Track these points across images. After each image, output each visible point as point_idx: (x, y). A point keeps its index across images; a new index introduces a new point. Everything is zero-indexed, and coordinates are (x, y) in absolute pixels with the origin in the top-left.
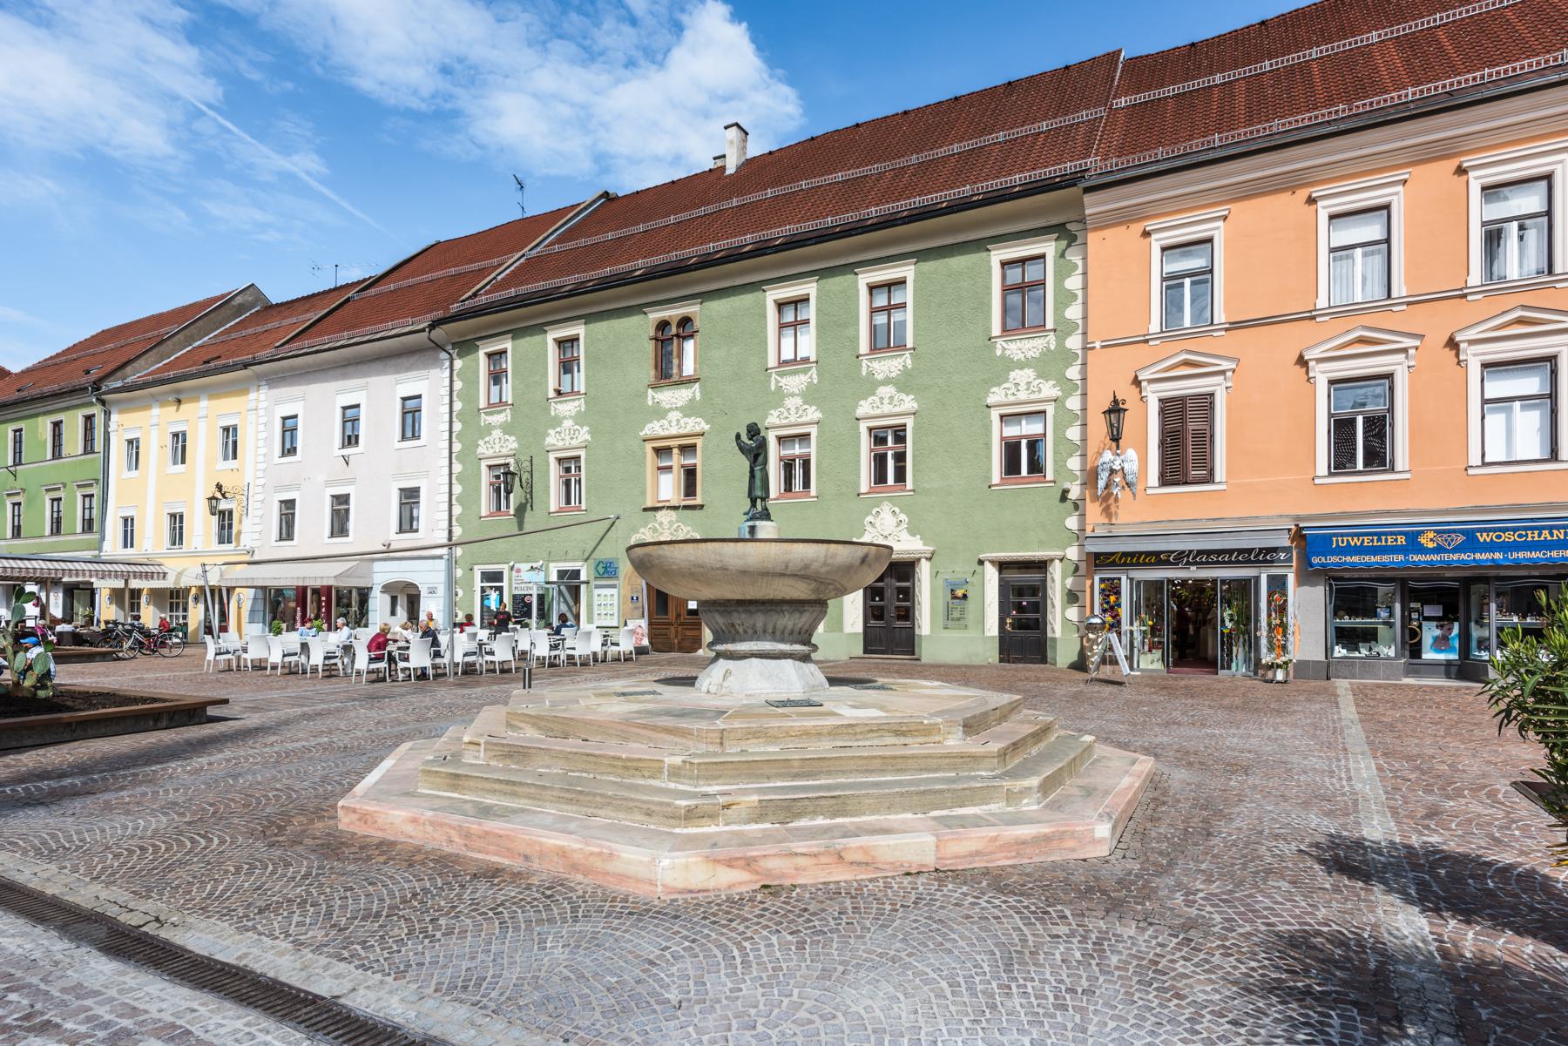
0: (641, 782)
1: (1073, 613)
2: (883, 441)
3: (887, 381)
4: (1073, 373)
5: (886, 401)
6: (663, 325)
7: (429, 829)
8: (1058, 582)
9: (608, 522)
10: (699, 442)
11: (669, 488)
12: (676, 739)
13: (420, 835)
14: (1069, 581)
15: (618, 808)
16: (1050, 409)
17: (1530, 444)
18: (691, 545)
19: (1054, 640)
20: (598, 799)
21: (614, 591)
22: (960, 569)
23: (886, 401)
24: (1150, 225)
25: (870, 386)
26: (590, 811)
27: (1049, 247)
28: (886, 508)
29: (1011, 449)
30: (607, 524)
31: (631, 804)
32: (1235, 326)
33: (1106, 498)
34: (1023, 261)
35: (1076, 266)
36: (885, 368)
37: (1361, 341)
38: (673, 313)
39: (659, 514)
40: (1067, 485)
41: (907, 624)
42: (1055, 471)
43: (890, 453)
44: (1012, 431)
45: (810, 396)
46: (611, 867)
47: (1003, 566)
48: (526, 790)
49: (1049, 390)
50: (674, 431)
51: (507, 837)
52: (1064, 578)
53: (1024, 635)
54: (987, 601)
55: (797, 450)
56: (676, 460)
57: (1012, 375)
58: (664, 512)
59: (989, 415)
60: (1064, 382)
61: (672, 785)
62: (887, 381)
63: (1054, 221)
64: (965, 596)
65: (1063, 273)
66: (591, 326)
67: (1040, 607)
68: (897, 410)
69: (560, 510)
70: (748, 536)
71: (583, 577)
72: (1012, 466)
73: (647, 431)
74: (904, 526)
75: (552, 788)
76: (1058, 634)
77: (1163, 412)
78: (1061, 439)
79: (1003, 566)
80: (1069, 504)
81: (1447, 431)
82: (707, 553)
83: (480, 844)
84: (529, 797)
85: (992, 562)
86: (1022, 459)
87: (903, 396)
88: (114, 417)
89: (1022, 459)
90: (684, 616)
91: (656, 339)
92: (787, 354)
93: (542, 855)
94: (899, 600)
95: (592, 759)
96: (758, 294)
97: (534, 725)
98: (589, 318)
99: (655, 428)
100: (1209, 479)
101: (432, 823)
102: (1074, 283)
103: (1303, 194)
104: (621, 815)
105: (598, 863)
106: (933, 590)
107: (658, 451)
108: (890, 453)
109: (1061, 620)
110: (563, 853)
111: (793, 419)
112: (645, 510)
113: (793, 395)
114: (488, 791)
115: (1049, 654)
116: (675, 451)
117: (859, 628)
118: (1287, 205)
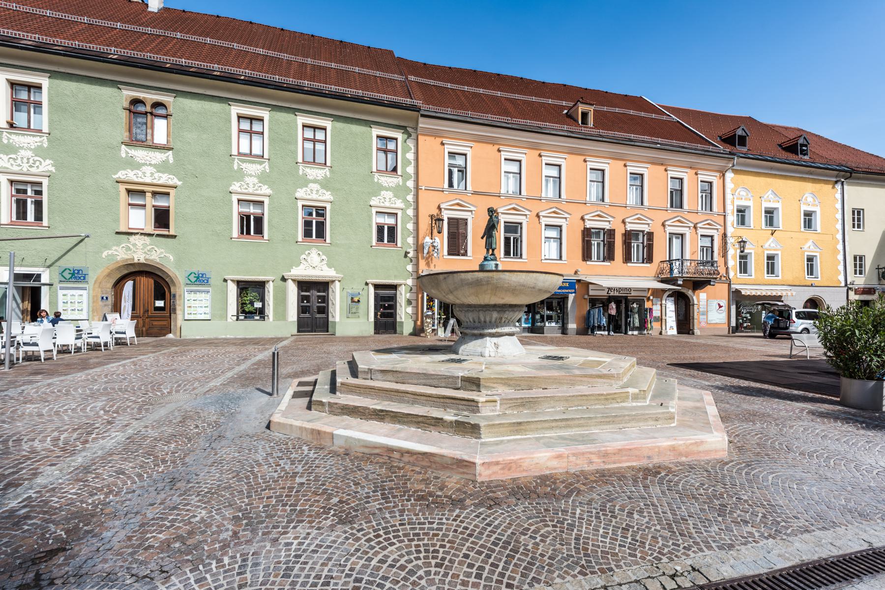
0: (617, 405)
1: (410, 310)
2: (311, 214)
3: (315, 181)
4: (410, 198)
5: (314, 192)
6: (136, 102)
7: (572, 459)
8: (403, 296)
9: (80, 239)
10: (172, 192)
12: (604, 381)
13: (565, 465)
14: (408, 295)
16: (400, 213)
19: (402, 323)
20: (627, 418)
21: (84, 293)
22: (357, 287)
23: (314, 192)
25: (305, 182)
26: (621, 426)
27: (399, 135)
28: (314, 253)
29: (380, 229)
30: (75, 240)
32: (475, 193)
33: (427, 259)
37: (458, 204)
38: (151, 97)
40: (408, 250)
42: (402, 243)
43: (29, 201)
45: (263, 178)
47: (377, 287)
48: (577, 422)
49: (399, 204)
50: (148, 180)
51: (635, 449)
53: (386, 320)
56: (150, 201)
57: (382, 193)
58: (138, 236)
59: (231, 197)
60: (406, 201)
61: (634, 404)
62: (315, 181)
66: (273, 113)
67: (393, 307)
68: (321, 198)
69: (12, 223)
71: (45, 279)
72: (380, 239)
73: (121, 175)
74: (325, 262)
75: (596, 418)
76: (337, 319)
77: (449, 224)
78: (404, 228)
79: (377, 287)
80: (408, 259)
81: (536, 248)
83: (616, 458)
84: (579, 426)
85: (233, 281)
87: (325, 191)
88: (845, 187)
89: (252, 225)
90: (152, 312)
91: (130, 111)
92: (245, 149)
94: (319, 302)
95: (584, 398)
96: (225, 106)
97: (505, 384)
98: (53, 75)
99: (130, 175)
100: (465, 254)
101: (574, 455)
102: (410, 156)
103: (496, 147)
104: (641, 424)
105: (695, 449)
106: (341, 297)
109: (405, 314)
110: (673, 449)
112: (117, 233)
113: (251, 176)
114: (547, 428)
115: (398, 329)
116: (149, 195)
117: (295, 318)
118: (491, 149)
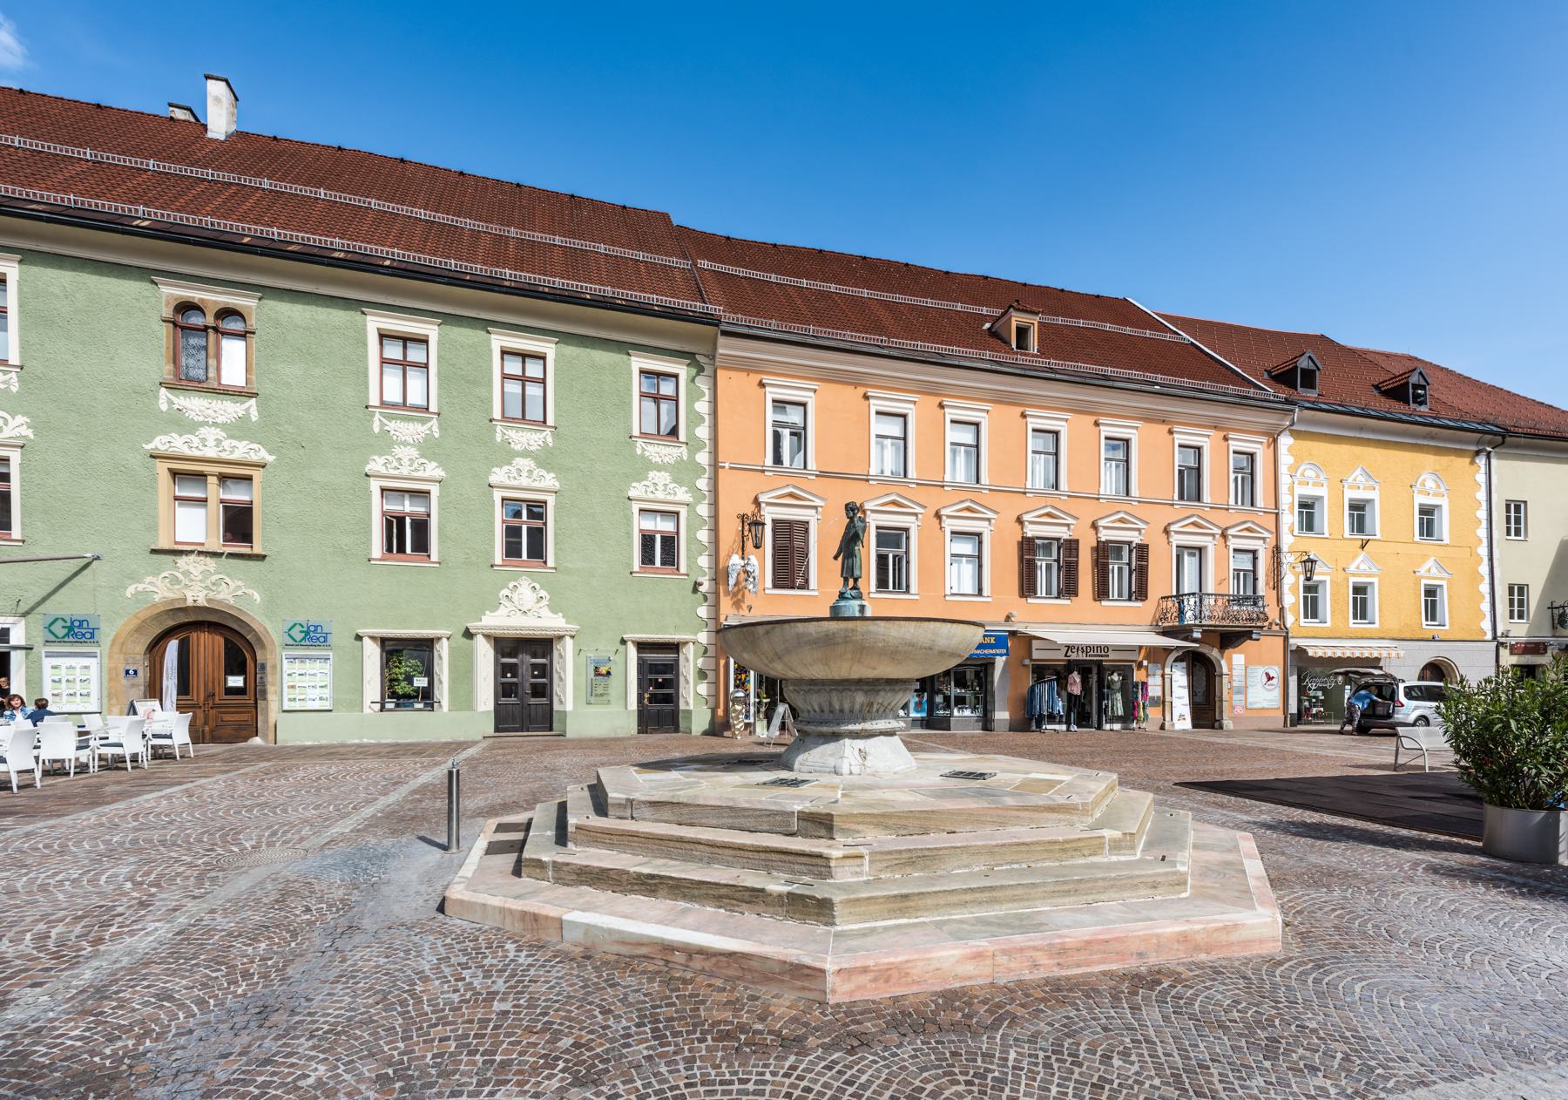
0: (1082, 861)
1: (703, 689)
2: (518, 514)
3: (525, 454)
4: (703, 483)
5: (525, 474)
6: (185, 307)
8: (690, 663)
10: (257, 475)
11: (196, 525)
12: (1060, 816)
14: (700, 661)
15: (1122, 888)
17: (969, 586)
18: (913, 624)
19: (689, 712)
20: (1100, 883)
23: (525, 474)
24: (1029, 411)
25: (506, 455)
26: (1090, 898)
27: (682, 370)
30: (74, 565)
31: (1137, 881)
32: (823, 475)
34: (524, 356)
35: (703, 394)
36: (524, 440)
39: (182, 561)
40: (700, 580)
41: (544, 701)
42: (688, 566)
43: (524, 528)
44: (649, 524)
45: (428, 449)
46: (1234, 937)
47: (642, 646)
48: (1009, 893)
49: (682, 495)
50: (211, 453)
52: (696, 659)
54: (367, 677)
55: (408, 507)
57: (651, 474)
58: (192, 557)
59: (368, 484)
60: (694, 489)
61: (1114, 858)
62: (525, 454)
63: (687, 348)
64: (609, 673)
65: (694, 396)
67: (673, 683)
68: (536, 485)
70: (857, 614)
72: (648, 558)
73: (160, 443)
74: (545, 602)
78: (692, 539)
79: (642, 646)
81: (935, 574)
82: (909, 631)
84: (1013, 900)
85: (373, 638)
86: (661, 550)
87: (543, 472)
88: (1494, 461)
89: (409, 535)
92: (392, 395)
93: (1159, 947)
94: (534, 677)
95: (1023, 848)
96: (356, 316)
99: (178, 443)
100: (805, 586)
102: (703, 407)
103: (861, 390)
105: (1223, 937)
107: (175, 474)
108: (524, 528)
109: (694, 696)
110: (1184, 938)
111: (405, 471)
112: (154, 551)
113: (405, 444)
116: (212, 480)
117: (491, 706)
118: (852, 394)
